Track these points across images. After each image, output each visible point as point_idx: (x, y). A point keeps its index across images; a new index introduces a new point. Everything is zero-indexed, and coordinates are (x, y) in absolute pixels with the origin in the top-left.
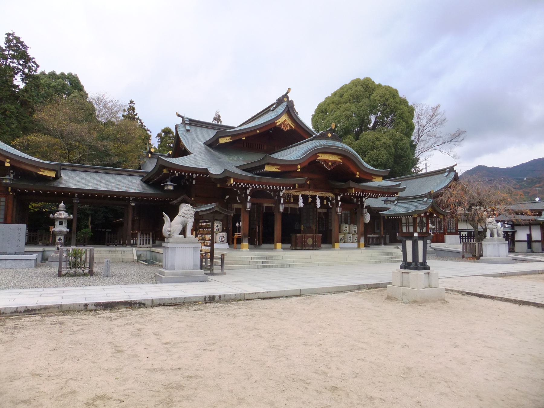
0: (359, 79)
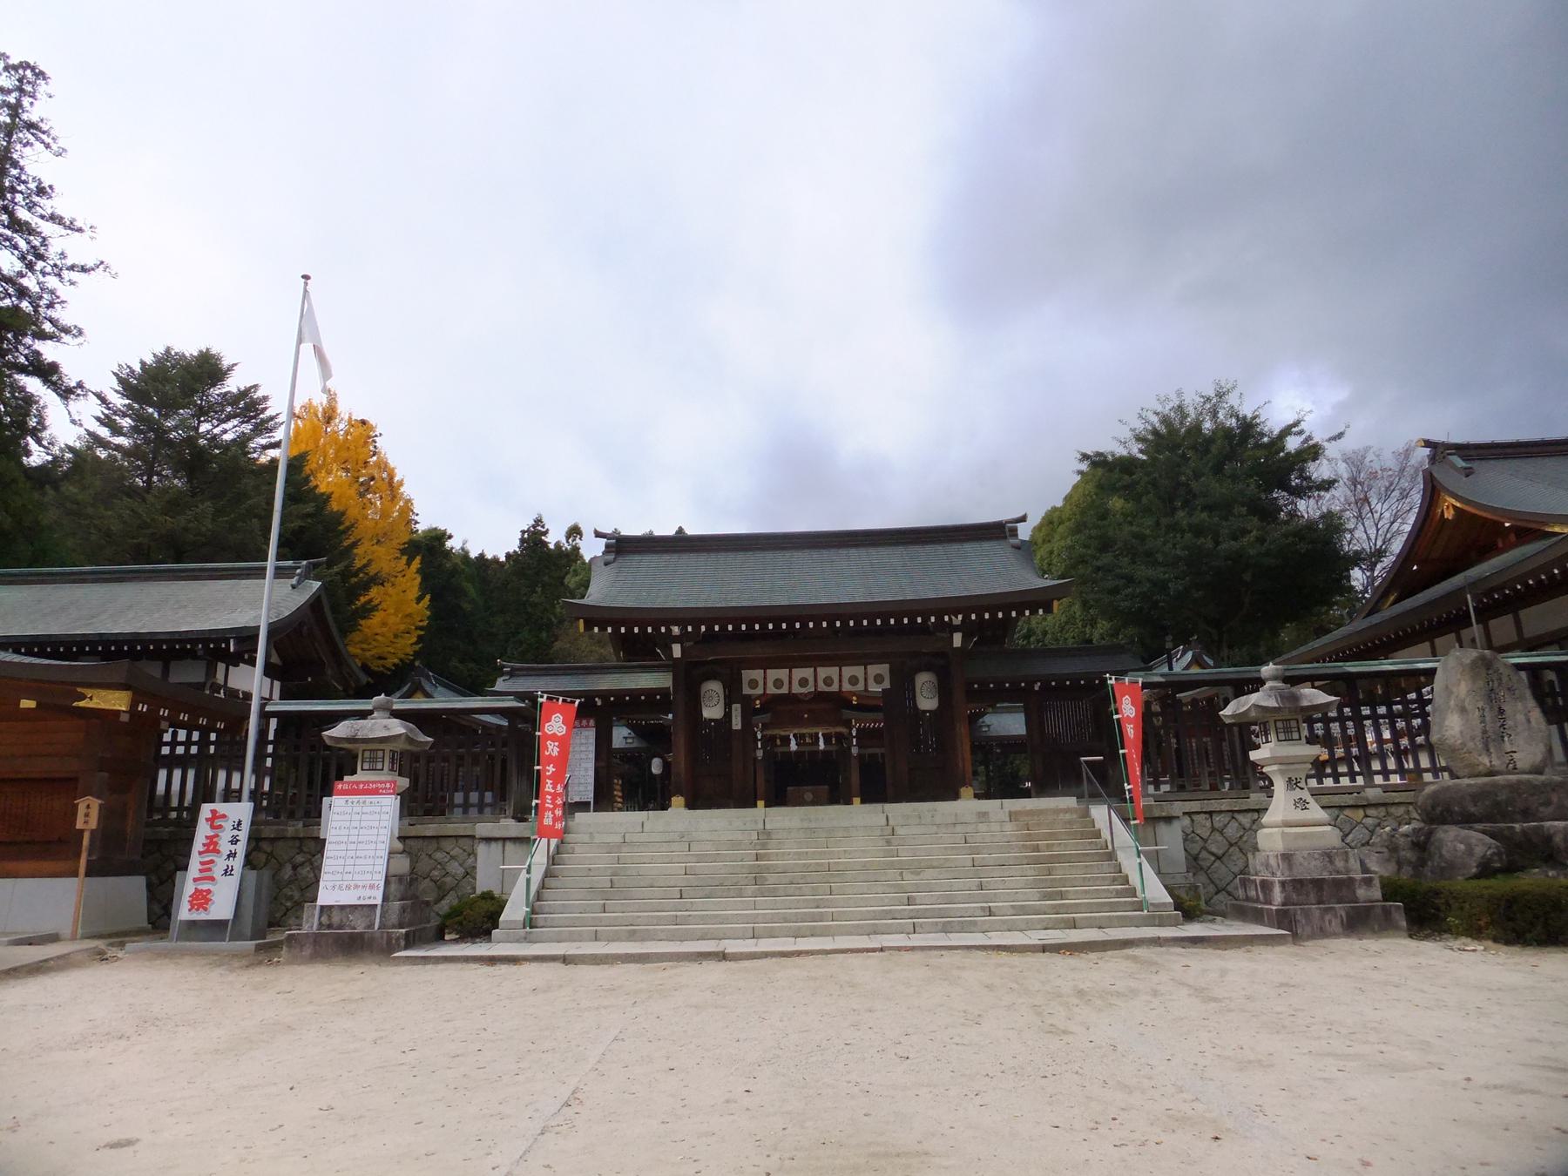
0: (1054, 509)
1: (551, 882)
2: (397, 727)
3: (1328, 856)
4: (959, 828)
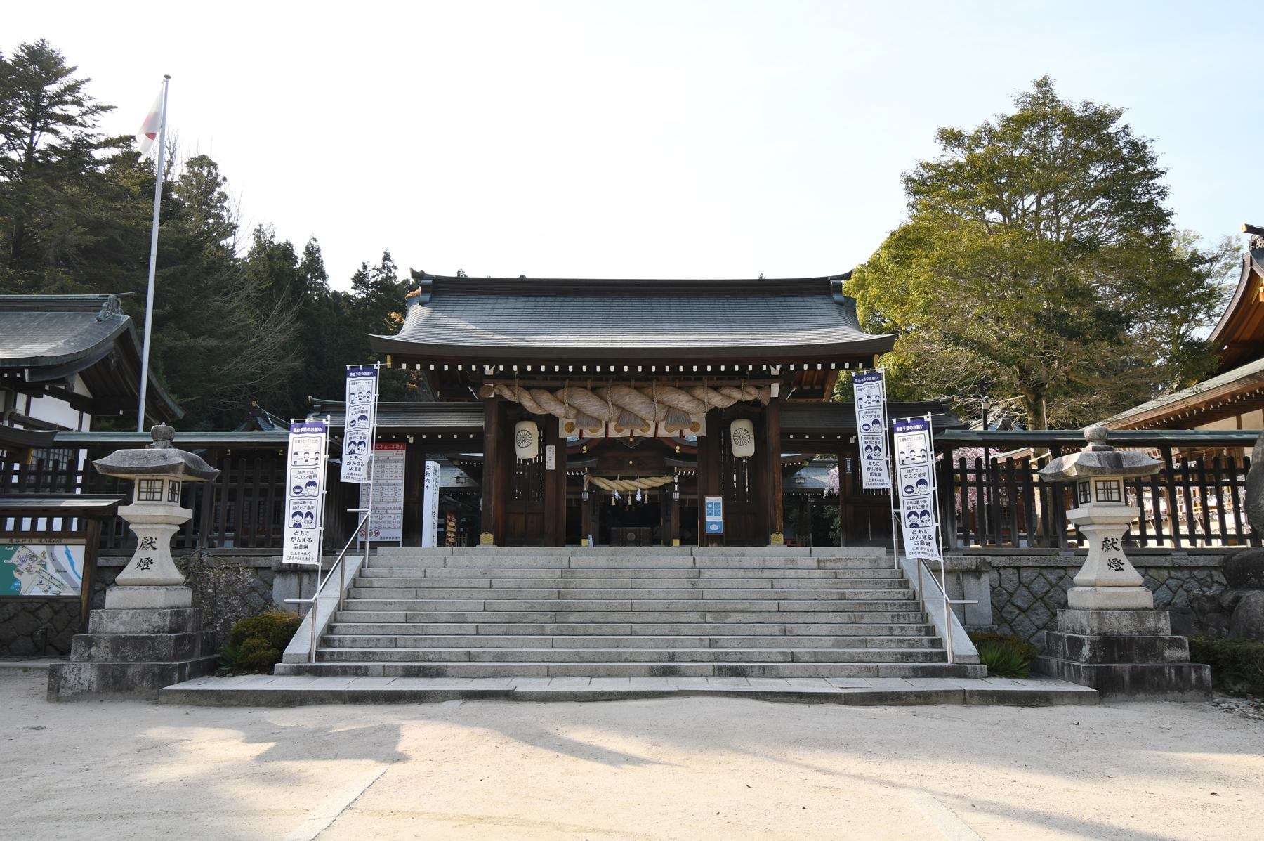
1: (346, 616)
2: (177, 457)
3: (1139, 613)
4: (766, 573)
